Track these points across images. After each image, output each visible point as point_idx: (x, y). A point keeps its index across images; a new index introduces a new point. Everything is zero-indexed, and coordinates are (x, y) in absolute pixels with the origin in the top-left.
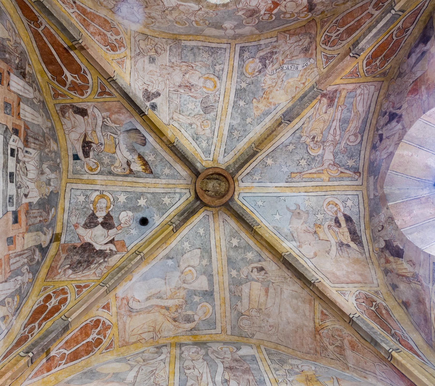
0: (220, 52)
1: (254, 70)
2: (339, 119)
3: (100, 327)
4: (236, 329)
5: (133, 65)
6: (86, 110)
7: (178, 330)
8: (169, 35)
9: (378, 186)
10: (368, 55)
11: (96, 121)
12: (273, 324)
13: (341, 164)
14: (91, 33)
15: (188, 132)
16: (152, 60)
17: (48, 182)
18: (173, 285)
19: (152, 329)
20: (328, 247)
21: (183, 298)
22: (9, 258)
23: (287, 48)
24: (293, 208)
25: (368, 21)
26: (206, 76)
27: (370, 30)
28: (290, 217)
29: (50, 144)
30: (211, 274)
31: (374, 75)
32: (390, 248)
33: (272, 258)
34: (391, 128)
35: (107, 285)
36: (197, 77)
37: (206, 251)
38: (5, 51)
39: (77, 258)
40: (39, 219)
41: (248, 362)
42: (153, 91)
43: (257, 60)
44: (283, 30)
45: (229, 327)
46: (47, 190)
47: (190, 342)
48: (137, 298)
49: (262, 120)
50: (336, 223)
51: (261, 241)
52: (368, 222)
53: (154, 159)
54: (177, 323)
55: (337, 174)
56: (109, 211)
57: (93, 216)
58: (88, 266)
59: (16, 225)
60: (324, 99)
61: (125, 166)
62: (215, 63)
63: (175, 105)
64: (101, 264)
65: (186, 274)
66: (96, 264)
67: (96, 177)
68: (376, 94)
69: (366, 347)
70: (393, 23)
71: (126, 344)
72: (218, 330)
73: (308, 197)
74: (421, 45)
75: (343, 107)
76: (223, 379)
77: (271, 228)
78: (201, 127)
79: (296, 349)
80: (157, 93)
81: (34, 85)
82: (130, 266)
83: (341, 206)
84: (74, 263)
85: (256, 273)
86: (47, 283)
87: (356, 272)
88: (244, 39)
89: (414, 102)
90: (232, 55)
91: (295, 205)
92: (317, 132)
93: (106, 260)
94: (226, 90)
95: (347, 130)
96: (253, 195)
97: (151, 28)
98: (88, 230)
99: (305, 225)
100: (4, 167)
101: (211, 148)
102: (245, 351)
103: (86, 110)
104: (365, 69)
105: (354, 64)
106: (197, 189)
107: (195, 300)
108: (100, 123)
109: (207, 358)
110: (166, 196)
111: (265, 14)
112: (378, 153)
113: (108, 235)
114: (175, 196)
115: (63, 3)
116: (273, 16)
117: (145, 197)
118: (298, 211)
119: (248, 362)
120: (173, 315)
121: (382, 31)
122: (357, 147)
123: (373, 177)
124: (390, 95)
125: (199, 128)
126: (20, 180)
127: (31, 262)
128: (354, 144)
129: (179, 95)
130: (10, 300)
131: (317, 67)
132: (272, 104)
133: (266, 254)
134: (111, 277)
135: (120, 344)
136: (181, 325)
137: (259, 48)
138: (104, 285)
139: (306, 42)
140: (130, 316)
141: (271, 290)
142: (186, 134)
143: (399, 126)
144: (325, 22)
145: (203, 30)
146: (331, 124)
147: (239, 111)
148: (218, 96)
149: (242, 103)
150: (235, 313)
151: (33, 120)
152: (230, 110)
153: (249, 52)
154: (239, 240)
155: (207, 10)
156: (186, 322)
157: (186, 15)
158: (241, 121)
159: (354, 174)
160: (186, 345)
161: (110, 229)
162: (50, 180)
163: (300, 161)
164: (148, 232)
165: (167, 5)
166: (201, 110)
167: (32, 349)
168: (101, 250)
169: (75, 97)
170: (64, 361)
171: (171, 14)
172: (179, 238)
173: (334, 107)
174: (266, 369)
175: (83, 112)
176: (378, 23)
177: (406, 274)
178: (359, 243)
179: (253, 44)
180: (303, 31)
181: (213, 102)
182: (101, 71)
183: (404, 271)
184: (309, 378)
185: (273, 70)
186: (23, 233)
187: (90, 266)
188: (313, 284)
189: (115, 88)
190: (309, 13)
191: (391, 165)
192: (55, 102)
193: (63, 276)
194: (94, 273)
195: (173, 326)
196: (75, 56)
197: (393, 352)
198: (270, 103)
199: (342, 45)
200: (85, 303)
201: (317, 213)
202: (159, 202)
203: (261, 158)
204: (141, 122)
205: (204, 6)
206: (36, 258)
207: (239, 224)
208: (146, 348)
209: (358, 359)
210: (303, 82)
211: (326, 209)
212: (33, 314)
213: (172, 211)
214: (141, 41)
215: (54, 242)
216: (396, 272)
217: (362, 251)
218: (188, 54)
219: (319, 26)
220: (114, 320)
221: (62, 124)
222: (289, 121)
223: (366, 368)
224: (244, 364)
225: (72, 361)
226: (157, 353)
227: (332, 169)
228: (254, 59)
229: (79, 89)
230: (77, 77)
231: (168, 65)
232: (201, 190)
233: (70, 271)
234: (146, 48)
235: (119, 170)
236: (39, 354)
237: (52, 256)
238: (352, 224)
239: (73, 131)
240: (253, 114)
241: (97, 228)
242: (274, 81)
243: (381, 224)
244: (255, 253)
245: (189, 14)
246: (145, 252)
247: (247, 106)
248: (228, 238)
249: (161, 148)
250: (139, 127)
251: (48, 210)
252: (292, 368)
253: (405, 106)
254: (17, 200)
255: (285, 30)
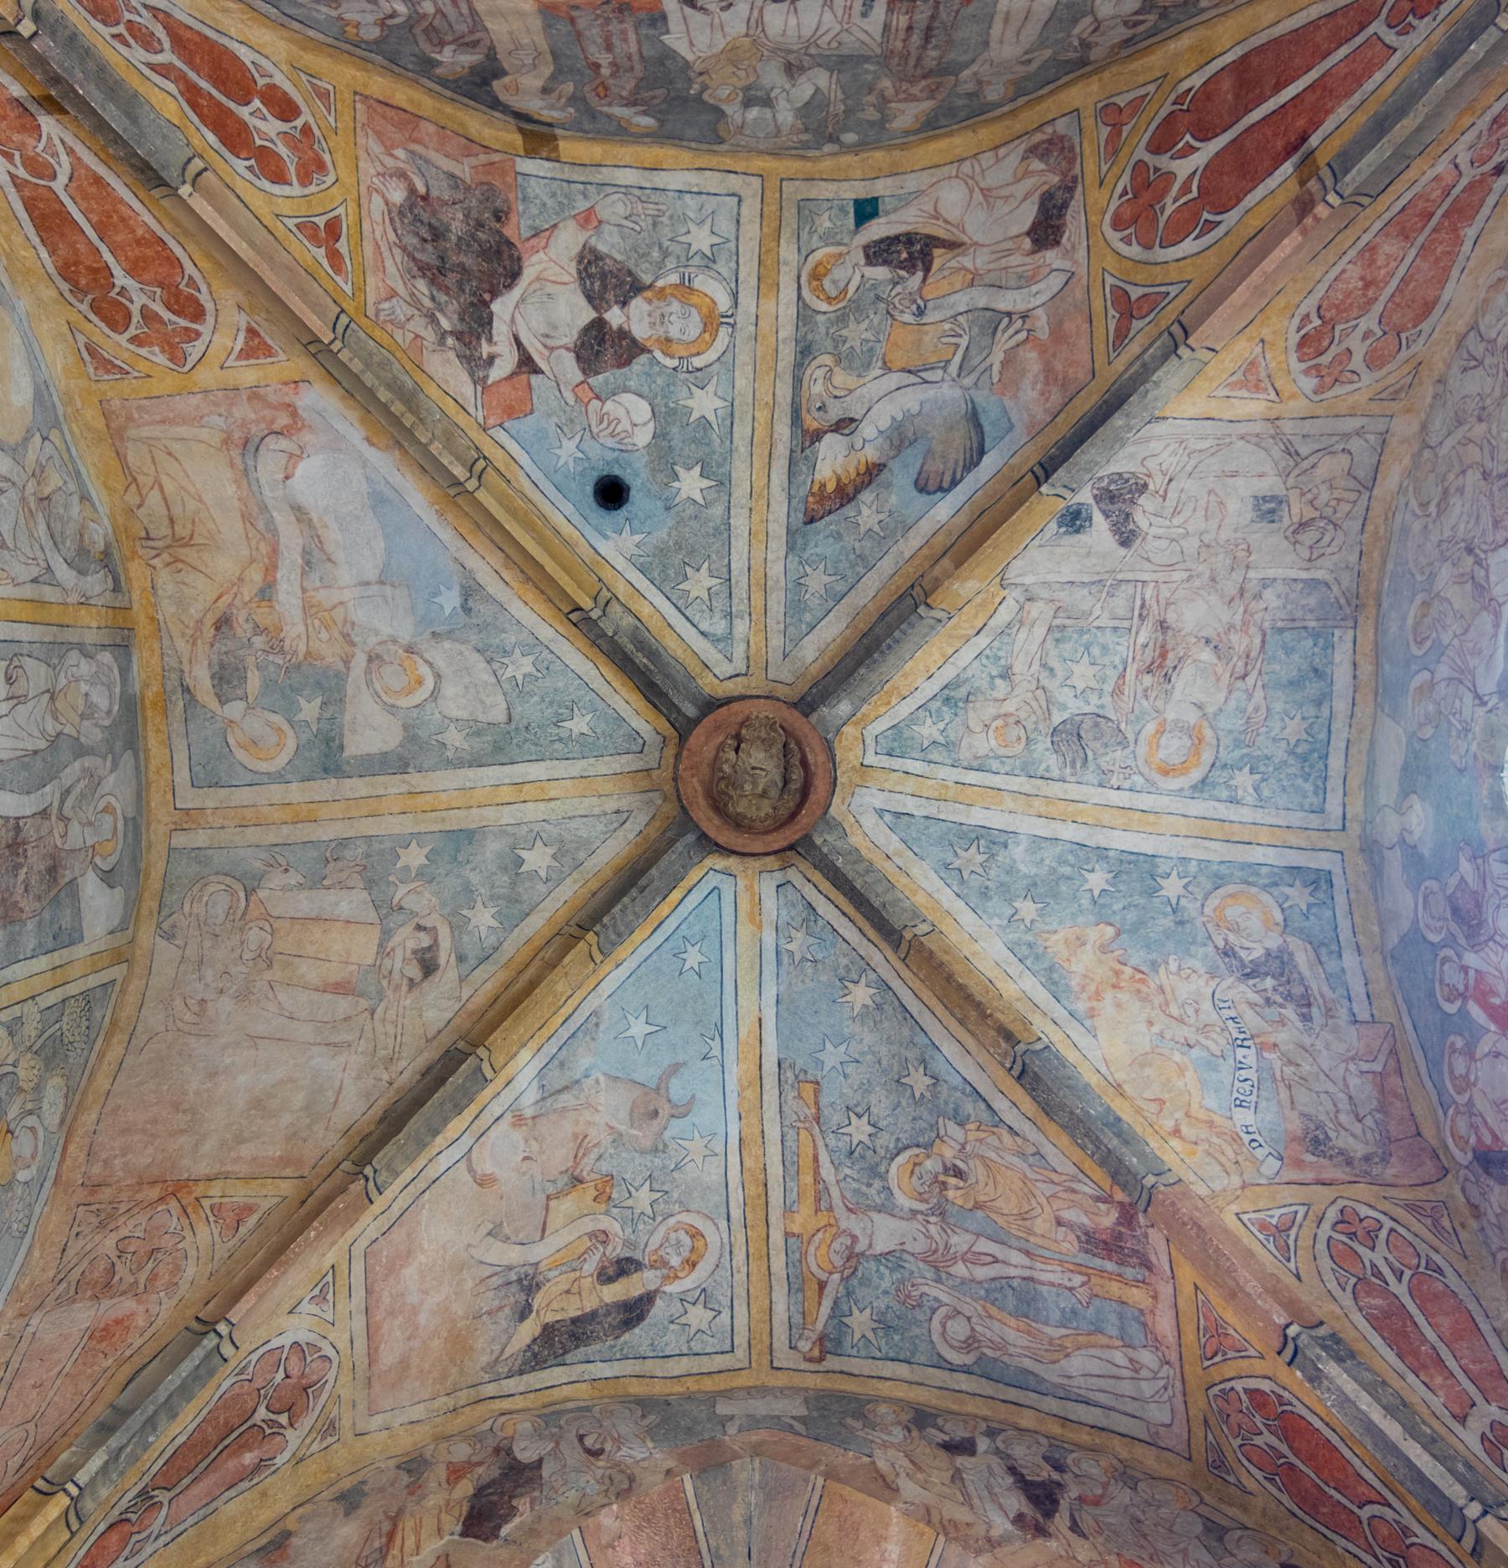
0: (1309, 787)
1: (1236, 929)
3: (174, 318)
5: (1242, 428)
6: (1057, 243)
11: (1012, 283)
12: (211, 1013)
13: (855, 1282)
14: (1371, 248)
15: (976, 664)
16: (1268, 509)
17: (755, 97)
18: (359, 615)
20: (517, 1231)
21: (308, 654)
23: (1325, 1064)
24: (677, 1089)
25: (1436, 1402)
26: (1208, 734)
27: (1399, 1409)
30: (407, 765)
31: (1212, 1421)
32: (508, 1485)
33: (470, 1006)
36: (1200, 697)
39: (457, 225)
40: (604, 59)
41: (46, 915)
43: (1274, 942)
44: (1399, 1046)
45: (200, 839)
46: (725, 92)
48: (301, 470)
50: (619, 1261)
51: (537, 963)
52: (621, 1392)
53: (863, 529)
55: (814, 1268)
57: (630, 288)
58: (423, 269)
60: (1114, 1215)
61: (835, 412)
63: (1085, 607)
64: (433, 319)
65: (406, 664)
66: (433, 299)
67: (788, 293)
68: (1137, 1429)
69: (98, 1388)
70: (1426, 1504)
71: (115, 432)
72: (189, 798)
73: (720, 1149)
75: (1083, 1294)
78: (996, 718)
79: (110, 1104)
80: (1132, 532)
81: (1151, 18)
83: (689, 1282)
84: (434, 213)
85: (411, 945)
86: (348, 101)
87: (416, 1343)
88: (1364, 887)
93: (450, 341)
94: (1152, 818)
95: (993, 1311)
97: (1402, 501)
98: (573, 268)
99: (606, 1139)
102: (99, 906)
103: (1057, 243)
104: (1238, 1385)
106: (747, 703)
107: (302, 702)
108: (1006, 301)
110: (716, 581)
111: (1465, 969)
112: (898, 1434)
113: (552, 349)
115: (1495, 121)
116: (1458, 1003)
117: (712, 495)
119: (46, 915)
120: (240, 617)
122: (923, 1346)
125: (992, 710)
127: (425, 31)
128: (935, 1337)
129: (1126, 624)
133: (486, 982)
134: (376, 359)
136: (202, 648)
137: (1324, 946)
138: (340, 329)
139: (1351, 1140)
140: (227, 441)
141: (343, 1005)
142: (967, 655)
143: (1001, 1525)
144: (1436, 1222)
147: (1066, 870)
148: (1127, 784)
149: (1097, 880)
150: (258, 864)
151: (1006, 20)
152: (1068, 832)
153: (1309, 906)
154: (543, 874)
157: (1456, 642)
158: (1026, 876)
159: (814, 1337)
160: (125, 671)
161: (578, 358)
162: (767, 102)
164: (568, 509)
165: (1494, 560)
166: (1066, 715)
167: (53, 34)
168: (490, 323)
169: (1105, 192)
170: (22, 173)
171: (1460, 580)
172: (546, 633)
173: (1083, 1258)
174: (15, 986)
175: (1046, 231)
176: (1424, 1447)
177: (395, 1552)
178: (535, 1355)
179: (1344, 924)
180: (1395, 1131)
181: (1102, 761)
183: (410, 1543)
189: (1146, 357)
190: (1470, 1155)
193: (380, 169)
194: (393, 294)
195: (197, 616)
197: (66, 1501)
198: (1098, 996)
199: (1338, 1292)
200: (259, 251)
201: (656, 1186)
202: (692, 552)
203: (877, 958)
205: (1493, 717)
206: (446, 55)
207: (609, 873)
208: (103, 510)
209: (56, 1356)
210: (1185, 1130)
211: (672, 1221)
212: (212, 44)
213: (654, 606)
214: (1344, 460)
215: (521, 130)
216: (411, 1507)
217: (503, 1369)
218: (1296, 657)
219: (1421, 1193)
220: (206, 376)
222: (1023, 1072)
224: (39, 898)
226: (83, 551)
227: (836, 1246)
229: (1140, 211)
231: (1251, 574)
232: (740, 719)
233: (398, 196)
234: (1318, 481)
235: (818, 389)
237: (462, 124)
238: (615, 1328)
239: (971, 192)
240: (1054, 926)
242: (1190, 1011)
243: (608, 1447)
244: (493, 940)
247: (1085, 902)
248: (554, 831)
249: (907, 555)
250: (990, 463)
251: (644, 102)
252: (21, 1090)
255: (1402, 1056)
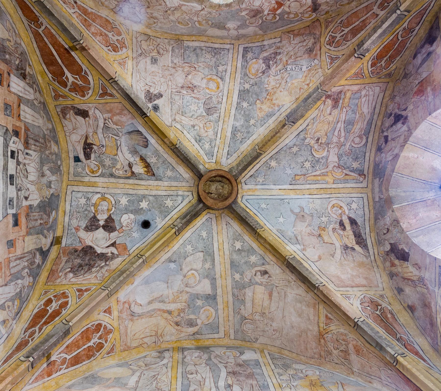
0: (223, 52)
1: (258, 70)
2: (343, 120)
3: (101, 331)
4: (239, 333)
5: (135, 66)
6: (87, 111)
7: (180, 334)
8: (171, 36)
9: (383, 189)
10: (374, 56)
11: (97, 122)
12: (276, 328)
13: (345, 166)
14: (93, 34)
15: (191, 134)
16: (154, 61)
17: (49, 185)
18: (176, 289)
19: (154, 333)
20: (332, 251)
21: (185, 302)
22: (9, 261)
23: (291, 49)
24: (297, 210)
25: (373, 21)
26: (209, 77)
27: (375, 30)
28: (294, 220)
29: (51, 146)
30: (214, 278)
31: (379, 76)
32: (396, 251)
33: (275, 262)
34: (396, 129)
35: (109, 289)
36: (200, 78)
37: (209, 254)
38: (5, 52)
39: (78, 261)
40: (39, 222)
41: (252, 367)
42: (155, 93)
43: (261, 61)
44: (287, 31)
45: (232, 332)
46: (48, 193)
47: (193, 346)
48: (139, 301)
49: (265, 121)
50: (340, 225)
51: (265, 244)
52: (373, 225)
53: (157, 161)
54: (179, 328)
55: (342, 176)
56: (111, 214)
57: (94, 219)
58: (89, 269)
59: (16, 227)
60: (328, 100)
61: (127, 168)
62: (218, 64)
63: (177, 106)
64: (102, 267)
65: (188, 277)
66: (97, 267)
67: (97, 179)
68: (381, 95)
69: (371, 352)
70: (398, 23)
71: (128, 349)
72: (221, 334)
73: (312, 200)
74: (427, 46)
75: (348, 109)
76: (226, 383)
77: (275, 231)
78: (204, 129)
79: (300, 354)
80: (159, 94)
81: (34, 86)
82: (132, 269)
83: (346, 208)
84: (75, 266)
85: (260, 277)
86: (47, 286)
87: (361, 276)
88: (248, 39)
89: (420, 103)
90: (235, 56)
91: (299, 207)
92: (321, 134)
93: (108, 263)
94: (230, 91)
95: (352, 131)
96: (256, 197)
97: (153, 28)
98: (89, 233)
99: (309, 228)
100: (4, 169)
101: (214, 150)
102: (248, 356)
103: (87, 111)
104: (370, 70)
105: (359, 65)
106: (200, 191)
107: (198, 304)
108: (101, 124)
109: (210, 362)
110: (168, 199)
111: (268, 14)
112: (383, 155)
113: (110, 238)
114: (177, 198)
115: (64, 3)
116: (277, 16)
117: (147, 199)
118: (302, 213)
119: (252, 367)
120: (176, 319)
121: (387, 32)
122: (361, 149)
123: (378, 179)
124: (396, 96)
125: (202, 130)
126: (20, 182)
127: (31, 265)
128: (359, 146)
129: (181, 96)
130: (10, 304)
131: (322, 68)
132: (276, 105)
133: (269, 258)
134: (112, 280)
135: (122, 348)
136: (184, 330)
137: (262, 49)
138: (105, 289)
139: (310, 42)
140: (132, 320)
141: (275, 294)
142: (188, 136)
143: (405, 128)
144: (330, 22)
145: (206, 31)
146: (335, 126)
147: (242, 112)
148: (221, 97)
149: (245, 105)
150: (239, 317)
151: (34, 121)
152: (233, 111)
153: (252, 53)
154: (242, 244)
155: (210, 10)
156: (189, 326)
157: (188, 15)
158: (244, 122)
159: (359, 177)
160: (189, 349)
161: (112, 232)
162: (50, 182)
163: (304, 163)
164: (150, 235)
165: (169, 6)
166: (204, 112)
167: (32, 354)
168: (103, 253)
169: (76, 99)
170: (65, 366)
171: (173, 14)
172: (181, 242)
173: (339, 108)
174: (270, 374)
175: (84, 114)
176: (384, 24)
177: (412, 278)
178: (364, 246)
179: (257, 44)
180: (308, 32)
181: (215, 103)
182: (102, 72)
183: (410, 274)
184: (314, 383)
185: (277, 71)
186: (24, 236)
187: (91, 269)
188: (318, 288)
189: (117, 89)
190: (314, 13)
191: (397, 167)
192: (56, 103)
193: (64, 279)
194: (96, 276)
195: (175, 330)
196: (76, 57)
197: (399, 356)
198: (274, 104)
199: (347, 45)
200: (86, 307)
201: (321, 216)
202: (161, 205)
203: (264, 160)
204: (143, 123)
205: (207, 6)
206: (37, 261)
207: (242, 227)
208: (148, 353)
209: (363, 363)
210: (307, 83)
211: (330, 212)
212: (33, 318)
213: (175, 214)
214: (143, 42)
215: (54, 245)
216: (401, 275)
217: (367, 254)
218: (191, 55)
219: (323, 26)
220: (115, 324)
221: (63, 126)
222: (293, 122)
223: (371, 373)
224: (247, 368)
225: (73, 365)
226: (159, 357)
227: (336, 171)
228: (258, 60)
229: (80, 90)
230: (78, 78)
231: (170, 65)
232: (204, 193)
233: (71, 275)
234: (148, 49)
235: (121, 172)
236: (39, 358)
237: (53, 260)
238: (357, 227)
239: (74, 133)
240: (256, 115)
241: (98, 231)
242: (278, 82)
243: (386, 227)
244: (259, 256)
245: (191, 14)
246: (147, 255)
247: (250, 107)
248: (231, 241)
249: (163, 150)
250: (141, 129)
251: (49, 213)
252: (296, 373)
253: (411, 107)
254: (17, 203)
255: (289, 30)
